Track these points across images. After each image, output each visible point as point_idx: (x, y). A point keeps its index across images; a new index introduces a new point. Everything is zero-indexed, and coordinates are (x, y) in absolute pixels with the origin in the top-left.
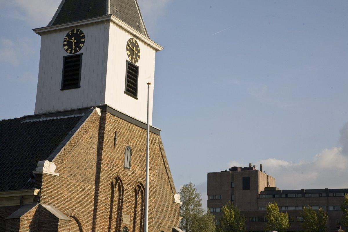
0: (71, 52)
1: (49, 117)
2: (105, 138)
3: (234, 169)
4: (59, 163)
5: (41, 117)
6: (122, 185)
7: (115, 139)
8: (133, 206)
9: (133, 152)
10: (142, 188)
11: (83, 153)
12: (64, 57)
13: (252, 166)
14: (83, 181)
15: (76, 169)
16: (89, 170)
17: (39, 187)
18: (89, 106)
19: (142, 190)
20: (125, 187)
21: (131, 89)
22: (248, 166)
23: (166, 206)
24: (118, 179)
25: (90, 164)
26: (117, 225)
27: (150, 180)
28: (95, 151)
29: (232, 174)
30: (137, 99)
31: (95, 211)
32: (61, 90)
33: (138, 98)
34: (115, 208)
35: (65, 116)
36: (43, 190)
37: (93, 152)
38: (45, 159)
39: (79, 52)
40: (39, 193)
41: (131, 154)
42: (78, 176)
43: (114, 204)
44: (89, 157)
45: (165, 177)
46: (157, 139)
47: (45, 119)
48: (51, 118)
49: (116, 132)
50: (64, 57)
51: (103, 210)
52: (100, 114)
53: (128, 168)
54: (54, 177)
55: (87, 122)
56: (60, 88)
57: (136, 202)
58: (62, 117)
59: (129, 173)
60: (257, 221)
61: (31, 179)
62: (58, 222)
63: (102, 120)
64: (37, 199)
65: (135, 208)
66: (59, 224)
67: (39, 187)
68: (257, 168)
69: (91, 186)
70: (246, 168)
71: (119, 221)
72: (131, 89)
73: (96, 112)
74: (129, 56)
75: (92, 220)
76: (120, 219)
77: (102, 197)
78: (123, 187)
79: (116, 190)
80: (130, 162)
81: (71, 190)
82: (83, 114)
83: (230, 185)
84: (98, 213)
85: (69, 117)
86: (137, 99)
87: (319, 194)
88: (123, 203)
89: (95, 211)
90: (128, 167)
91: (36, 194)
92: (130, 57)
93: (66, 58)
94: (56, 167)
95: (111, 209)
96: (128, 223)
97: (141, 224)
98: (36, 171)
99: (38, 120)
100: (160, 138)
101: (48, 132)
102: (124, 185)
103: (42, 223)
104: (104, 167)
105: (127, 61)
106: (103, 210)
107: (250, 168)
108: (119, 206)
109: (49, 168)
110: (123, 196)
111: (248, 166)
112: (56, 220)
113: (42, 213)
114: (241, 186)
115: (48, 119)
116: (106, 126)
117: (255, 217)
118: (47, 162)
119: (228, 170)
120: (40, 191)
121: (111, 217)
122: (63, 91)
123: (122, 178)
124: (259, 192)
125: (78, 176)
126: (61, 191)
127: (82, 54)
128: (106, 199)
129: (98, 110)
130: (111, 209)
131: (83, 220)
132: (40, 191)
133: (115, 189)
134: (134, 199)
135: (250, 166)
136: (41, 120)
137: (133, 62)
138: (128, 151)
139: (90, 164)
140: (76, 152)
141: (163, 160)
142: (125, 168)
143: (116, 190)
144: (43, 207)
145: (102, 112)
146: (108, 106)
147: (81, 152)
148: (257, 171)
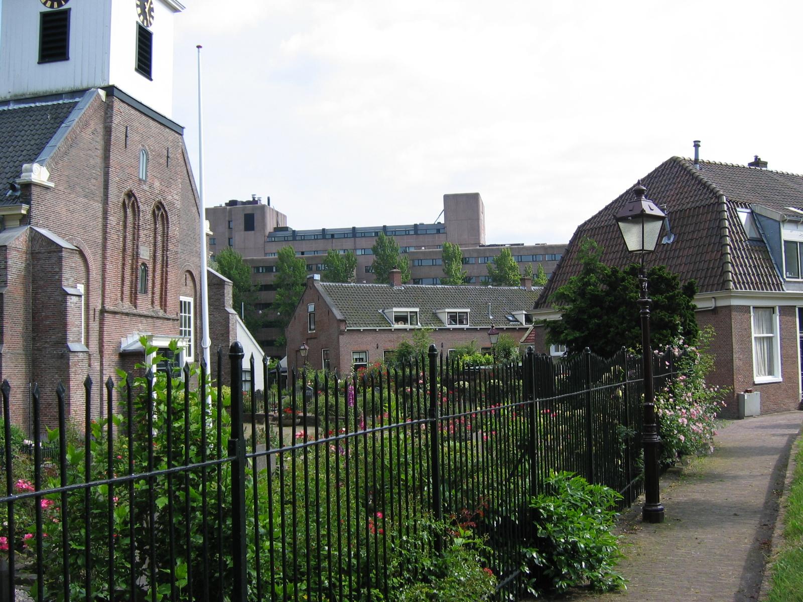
0: (52, 6)
1: (23, 103)
2: (113, 134)
3: (233, 203)
4: (52, 168)
5: (10, 104)
6: (137, 205)
7: (126, 136)
8: (152, 235)
9: (150, 157)
10: (162, 210)
11: (83, 156)
12: (41, 13)
13: (256, 199)
14: (85, 196)
15: (76, 179)
16: (93, 181)
17: (28, 202)
18: (85, 86)
19: (162, 213)
20: (142, 207)
21: (144, 65)
22: (251, 199)
23: (192, 236)
24: (130, 194)
25: (94, 171)
26: (132, 260)
27: (174, 198)
28: (100, 153)
29: (230, 211)
30: (151, 80)
31: (105, 239)
32: (39, 63)
33: (153, 78)
34: (129, 237)
35: (48, 102)
36: (34, 207)
37: (96, 154)
38: (31, 161)
39: (66, 7)
40: (29, 211)
41: (147, 160)
42: (78, 189)
43: (128, 230)
44: (92, 162)
45: (191, 196)
46: (180, 140)
47: (16, 107)
48: (27, 106)
49: (127, 127)
50: (41, 13)
51: (115, 238)
52: (104, 98)
53: (144, 181)
54: (47, 188)
55: (75, 117)
56: (37, 59)
57: (156, 229)
58: (44, 104)
59: (146, 187)
60: (264, 271)
61: (11, 191)
62: (61, 251)
63: (108, 108)
64: (25, 220)
65: (155, 238)
66: (64, 254)
67: (28, 202)
68: (264, 202)
69: (96, 204)
70: (248, 202)
71: (136, 256)
72: (144, 65)
73: (99, 95)
74: (139, 15)
75: (100, 252)
76: (137, 253)
77: (113, 220)
78: (138, 207)
79: (129, 211)
80: (146, 172)
81: (71, 208)
82: (77, 100)
83: (227, 226)
84: (109, 243)
85: (55, 103)
86: (151, 80)
87: (701, 158)
88: (139, 229)
89: (105, 239)
90: (144, 179)
91: (24, 212)
92: (142, 17)
93: (45, 17)
94: (49, 174)
95: (125, 237)
96: (148, 258)
97: (163, 260)
98: (22, 178)
99: (6, 108)
100: (183, 139)
101: (38, 120)
102: (140, 204)
103: (37, 253)
104: (114, 178)
105: (137, 22)
106: (115, 238)
107: (254, 202)
108: (134, 234)
109: (39, 173)
110: (139, 220)
111: (251, 199)
112: (60, 248)
113: (35, 238)
114: (242, 227)
115: (22, 106)
116: (114, 118)
117: (262, 267)
118: (36, 166)
119: (224, 205)
120: (30, 207)
121: (124, 250)
122: (42, 66)
123: (137, 195)
124: (267, 234)
125: (78, 189)
126: (58, 209)
127: (70, 9)
128: (118, 224)
129: (102, 93)
130: (125, 237)
131: (88, 253)
132: (30, 207)
133: (128, 210)
134: (153, 225)
135: (254, 198)
136: (10, 108)
137: (145, 24)
138: (143, 155)
139: (94, 171)
140: (74, 154)
141: (187, 171)
142: (140, 180)
143: (129, 211)
144: (37, 231)
145: (107, 95)
146: (116, 88)
147: (81, 154)
148: (264, 206)
